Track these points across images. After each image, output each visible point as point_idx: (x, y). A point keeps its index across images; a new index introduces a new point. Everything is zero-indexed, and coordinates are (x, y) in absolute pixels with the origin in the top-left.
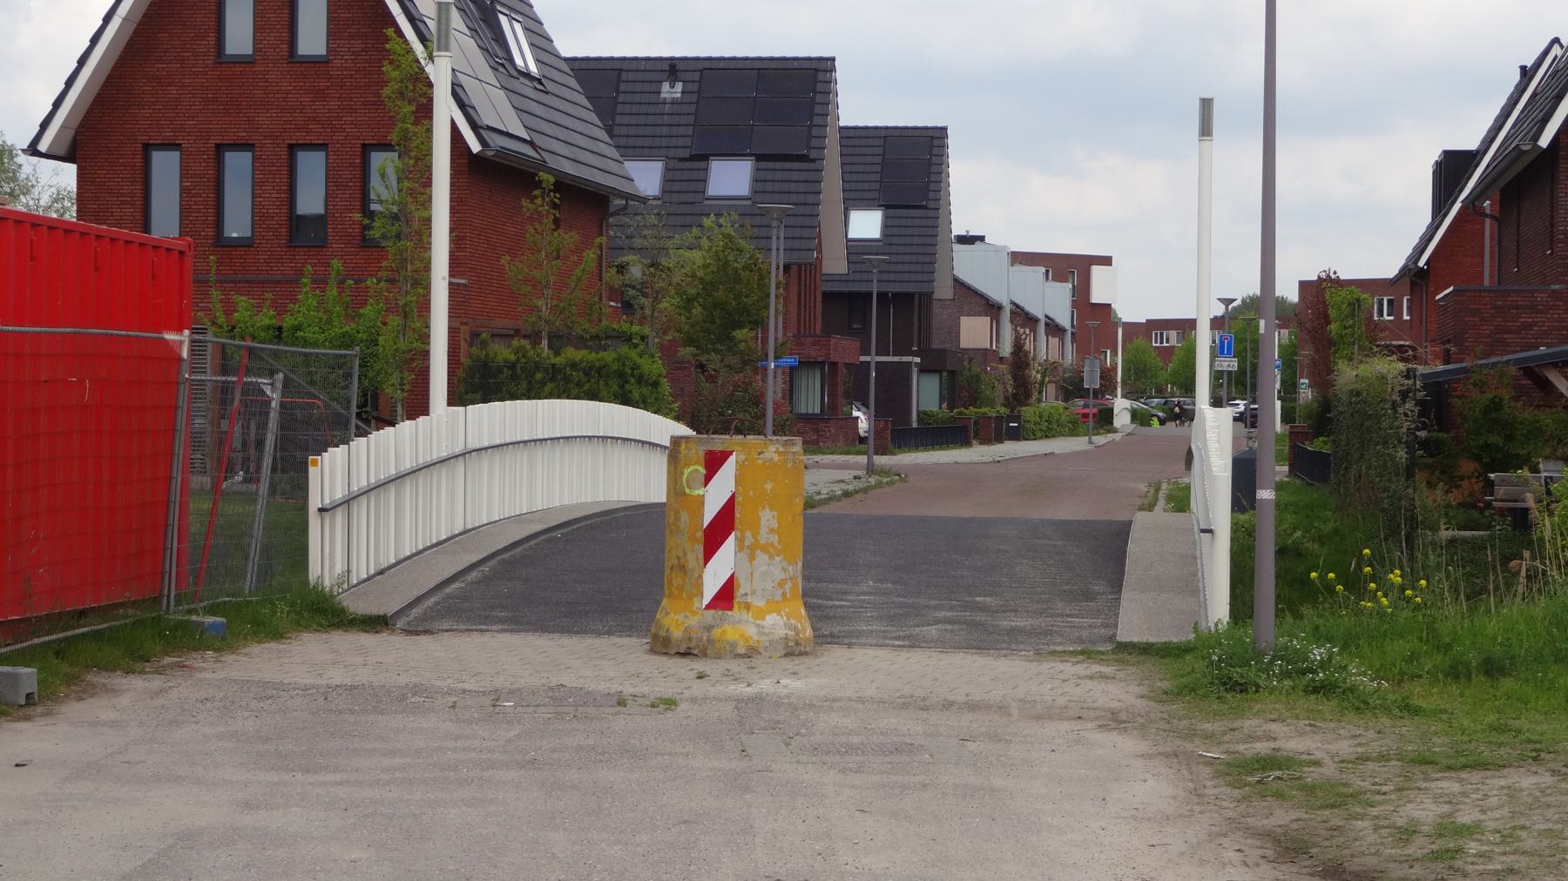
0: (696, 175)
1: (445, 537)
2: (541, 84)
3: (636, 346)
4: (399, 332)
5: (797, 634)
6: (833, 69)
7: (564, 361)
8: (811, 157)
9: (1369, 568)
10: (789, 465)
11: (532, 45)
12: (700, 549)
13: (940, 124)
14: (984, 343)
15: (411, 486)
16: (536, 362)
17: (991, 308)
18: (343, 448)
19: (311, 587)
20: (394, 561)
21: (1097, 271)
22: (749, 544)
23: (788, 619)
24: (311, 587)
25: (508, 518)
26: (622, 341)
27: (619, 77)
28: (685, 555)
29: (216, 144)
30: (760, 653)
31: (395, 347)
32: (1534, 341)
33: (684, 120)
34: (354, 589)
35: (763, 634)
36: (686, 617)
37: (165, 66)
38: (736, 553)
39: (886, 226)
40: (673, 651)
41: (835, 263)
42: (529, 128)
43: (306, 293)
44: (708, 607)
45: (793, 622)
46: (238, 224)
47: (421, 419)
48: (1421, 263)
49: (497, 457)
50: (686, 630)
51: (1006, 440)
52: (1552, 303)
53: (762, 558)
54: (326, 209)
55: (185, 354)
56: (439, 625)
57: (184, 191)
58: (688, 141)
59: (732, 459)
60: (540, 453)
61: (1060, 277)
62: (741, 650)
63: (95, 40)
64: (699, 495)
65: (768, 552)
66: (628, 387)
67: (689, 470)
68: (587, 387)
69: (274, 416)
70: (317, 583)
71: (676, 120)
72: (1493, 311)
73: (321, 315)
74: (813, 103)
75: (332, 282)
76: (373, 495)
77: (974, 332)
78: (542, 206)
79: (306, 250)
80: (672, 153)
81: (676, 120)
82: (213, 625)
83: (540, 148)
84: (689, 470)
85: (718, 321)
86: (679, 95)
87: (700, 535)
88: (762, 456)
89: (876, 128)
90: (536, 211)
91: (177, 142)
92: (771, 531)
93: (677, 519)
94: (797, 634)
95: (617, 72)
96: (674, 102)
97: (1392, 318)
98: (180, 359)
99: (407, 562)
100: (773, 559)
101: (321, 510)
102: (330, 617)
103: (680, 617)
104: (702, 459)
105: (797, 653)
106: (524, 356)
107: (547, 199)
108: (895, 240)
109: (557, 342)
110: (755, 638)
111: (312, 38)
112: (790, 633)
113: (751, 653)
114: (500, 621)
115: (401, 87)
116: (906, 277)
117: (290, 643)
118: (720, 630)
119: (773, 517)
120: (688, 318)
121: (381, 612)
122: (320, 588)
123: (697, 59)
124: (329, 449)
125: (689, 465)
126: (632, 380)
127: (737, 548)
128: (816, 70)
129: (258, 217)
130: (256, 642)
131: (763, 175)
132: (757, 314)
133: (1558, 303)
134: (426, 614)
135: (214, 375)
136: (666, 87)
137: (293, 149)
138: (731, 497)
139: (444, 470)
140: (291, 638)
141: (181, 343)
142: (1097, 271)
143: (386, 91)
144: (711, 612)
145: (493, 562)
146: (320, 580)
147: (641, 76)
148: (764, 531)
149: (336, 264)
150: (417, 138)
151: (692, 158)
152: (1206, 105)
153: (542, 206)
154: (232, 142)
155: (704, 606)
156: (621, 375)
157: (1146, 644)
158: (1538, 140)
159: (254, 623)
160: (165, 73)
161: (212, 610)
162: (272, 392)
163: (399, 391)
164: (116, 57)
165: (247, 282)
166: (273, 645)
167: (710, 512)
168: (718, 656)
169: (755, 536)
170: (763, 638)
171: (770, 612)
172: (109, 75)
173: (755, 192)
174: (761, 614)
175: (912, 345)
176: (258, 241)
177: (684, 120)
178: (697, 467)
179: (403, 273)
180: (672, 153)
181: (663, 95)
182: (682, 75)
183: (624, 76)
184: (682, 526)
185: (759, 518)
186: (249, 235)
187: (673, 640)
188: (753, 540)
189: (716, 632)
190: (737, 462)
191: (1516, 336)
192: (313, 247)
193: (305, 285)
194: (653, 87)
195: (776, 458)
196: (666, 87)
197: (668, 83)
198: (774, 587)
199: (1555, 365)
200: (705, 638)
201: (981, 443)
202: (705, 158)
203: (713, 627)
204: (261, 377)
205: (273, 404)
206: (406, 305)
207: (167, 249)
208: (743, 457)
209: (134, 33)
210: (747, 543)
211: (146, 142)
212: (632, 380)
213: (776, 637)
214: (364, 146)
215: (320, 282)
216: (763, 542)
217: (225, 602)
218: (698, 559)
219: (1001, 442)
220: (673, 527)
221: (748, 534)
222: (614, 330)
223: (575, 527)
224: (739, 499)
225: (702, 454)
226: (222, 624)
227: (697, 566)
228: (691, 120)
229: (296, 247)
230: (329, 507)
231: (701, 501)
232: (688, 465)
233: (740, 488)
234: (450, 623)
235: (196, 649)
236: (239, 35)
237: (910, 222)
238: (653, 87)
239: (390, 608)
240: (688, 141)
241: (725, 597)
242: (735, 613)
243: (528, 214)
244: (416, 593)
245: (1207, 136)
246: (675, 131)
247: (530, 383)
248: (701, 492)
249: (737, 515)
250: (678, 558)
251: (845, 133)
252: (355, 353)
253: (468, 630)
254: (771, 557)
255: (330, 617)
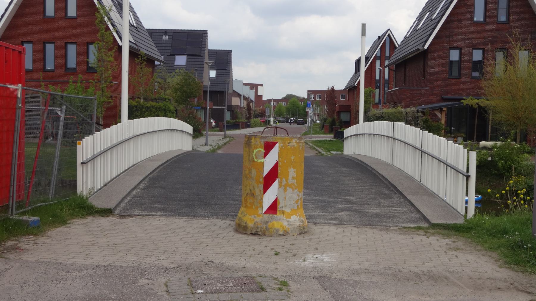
0: (172, 59)
1: (127, 168)
2: (137, 29)
3: (167, 102)
4: (100, 96)
5: (304, 224)
6: (207, 33)
7: (150, 106)
8: (202, 55)
9: (508, 188)
10: (301, 148)
11: (135, 19)
12: (261, 186)
13: (230, 49)
14: (237, 104)
15: (116, 150)
16: (143, 106)
17: (239, 95)
18: (91, 137)
19: (78, 196)
20: (110, 180)
21: (259, 87)
22: (284, 184)
23: (300, 217)
24: (78, 196)
25: (146, 159)
26: (163, 100)
27: (152, 34)
28: (254, 189)
29: (43, 42)
30: (289, 234)
31: (99, 100)
32: (421, 103)
33: (169, 45)
34: (95, 194)
35: (291, 225)
36: (255, 217)
37: (28, 18)
38: (278, 188)
39: (217, 74)
40: (250, 232)
41: (206, 83)
42: (135, 40)
43: (71, 85)
44: (265, 213)
45: (302, 218)
46: (50, 66)
47: (119, 124)
48: (355, 85)
49: (143, 137)
50: (255, 223)
51: (248, 127)
52: (426, 93)
53: (289, 190)
54: (76, 67)
55: (19, 95)
56: (134, 213)
57: (34, 55)
58: (170, 51)
59: (277, 146)
60: (156, 136)
61: (251, 89)
62: (281, 233)
63: (6, 10)
64: (261, 162)
65: (292, 188)
66: (166, 113)
67: (256, 150)
68: (156, 113)
69: (62, 123)
70: (81, 194)
71: (167, 45)
72: (410, 95)
73: (75, 91)
74: (202, 42)
75: (79, 81)
76: (102, 155)
77: (235, 101)
78: (141, 60)
79: (70, 73)
80: (166, 54)
81: (167, 45)
82: (34, 222)
83: (139, 46)
84: (256, 150)
85: (184, 96)
86: (167, 39)
87: (262, 180)
88: (290, 144)
89: (214, 50)
90: (139, 62)
91: (32, 41)
92: (293, 178)
93: (250, 172)
94: (304, 224)
95: (151, 33)
96: (166, 41)
97: (314, 99)
98: (17, 97)
99: (115, 180)
100: (294, 191)
101: (82, 163)
102: (87, 210)
103: (252, 217)
104: (263, 146)
105: (303, 232)
106: (139, 104)
107: (143, 59)
108: (219, 78)
109: (146, 99)
110: (287, 227)
111: (72, 11)
112: (301, 224)
113: (286, 233)
114: (160, 210)
115: (101, 20)
116: (222, 87)
117: (70, 227)
118: (271, 224)
119: (294, 172)
120: (176, 95)
121: (109, 207)
122: (82, 196)
123: (172, 30)
124: (85, 137)
125: (256, 148)
126: (168, 112)
127: (279, 186)
128: (203, 33)
129: (56, 63)
130: (54, 227)
131: (190, 60)
132: (195, 94)
133: (427, 93)
134: (126, 207)
135: (43, 107)
136: (164, 37)
137: (66, 44)
138: (277, 162)
139: (127, 143)
140: (69, 223)
141: (17, 90)
142: (259, 87)
143: (97, 21)
144: (267, 215)
145: (147, 179)
146: (82, 192)
147: (157, 34)
148: (290, 178)
149: (80, 76)
150: (106, 36)
151: (171, 55)
152: (364, 25)
153: (141, 60)
154: (48, 41)
155: (263, 213)
156: (165, 110)
157: (446, 224)
158: (424, 47)
159: (53, 216)
160: (28, 21)
161: (33, 212)
162: (61, 113)
163: (101, 114)
164: (13, 15)
165: (52, 82)
166: (61, 229)
167: (267, 169)
168: (271, 236)
169: (287, 180)
170: (290, 227)
171: (292, 215)
172: (11, 21)
173: (187, 64)
174: (289, 216)
175: (223, 104)
176: (56, 70)
177: (169, 45)
178: (260, 149)
179: (102, 77)
180: (166, 54)
181: (163, 39)
182: (168, 34)
183: (153, 34)
184: (253, 175)
185: (288, 172)
186: (53, 68)
187: (249, 228)
188: (286, 183)
189: (270, 225)
190: (279, 147)
191: (416, 102)
192: (72, 72)
193: (71, 82)
194: (161, 37)
195: (296, 145)
196: (164, 37)
197: (164, 36)
198: (294, 203)
199: (438, 110)
200: (264, 227)
201: (242, 129)
202: (174, 55)
203: (268, 222)
204: (56, 107)
205: (62, 118)
206: (103, 87)
207: (13, 50)
208: (282, 145)
209: (18, 8)
210: (283, 184)
211: (22, 41)
212: (168, 112)
213: (296, 226)
214: (87, 43)
215: (75, 82)
216: (290, 183)
217: (40, 206)
218: (260, 191)
219: (246, 128)
220: (248, 176)
221: (284, 180)
222: (161, 97)
223: (170, 162)
224: (280, 164)
225: (263, 143)
226: (38, 220)
227: (260, 194)
228: (170, 45)
229: (68, 72)
230: (85, 162)
231: (262, 164)
232: (256, 148)
233: (280, 159)
234: (138, 211)
235: (25, 235)
236: (50, 9)
237: (223, 73)
238: (161, 37)
239: (111, 205)
240: (170, 51)
241: (273, 208)
242: (278, 216)
243: (137, 63)
244: (122, 196)
245: (364, 36)
246: (166, 48)
247: (141, 112)
248: (262, 160)
249: (279, 171)
250: (251, 190)
251: (210, 51)
252: (95, 98)
253: (147, 215)
254: (293, 190)
255: (87, 210)
